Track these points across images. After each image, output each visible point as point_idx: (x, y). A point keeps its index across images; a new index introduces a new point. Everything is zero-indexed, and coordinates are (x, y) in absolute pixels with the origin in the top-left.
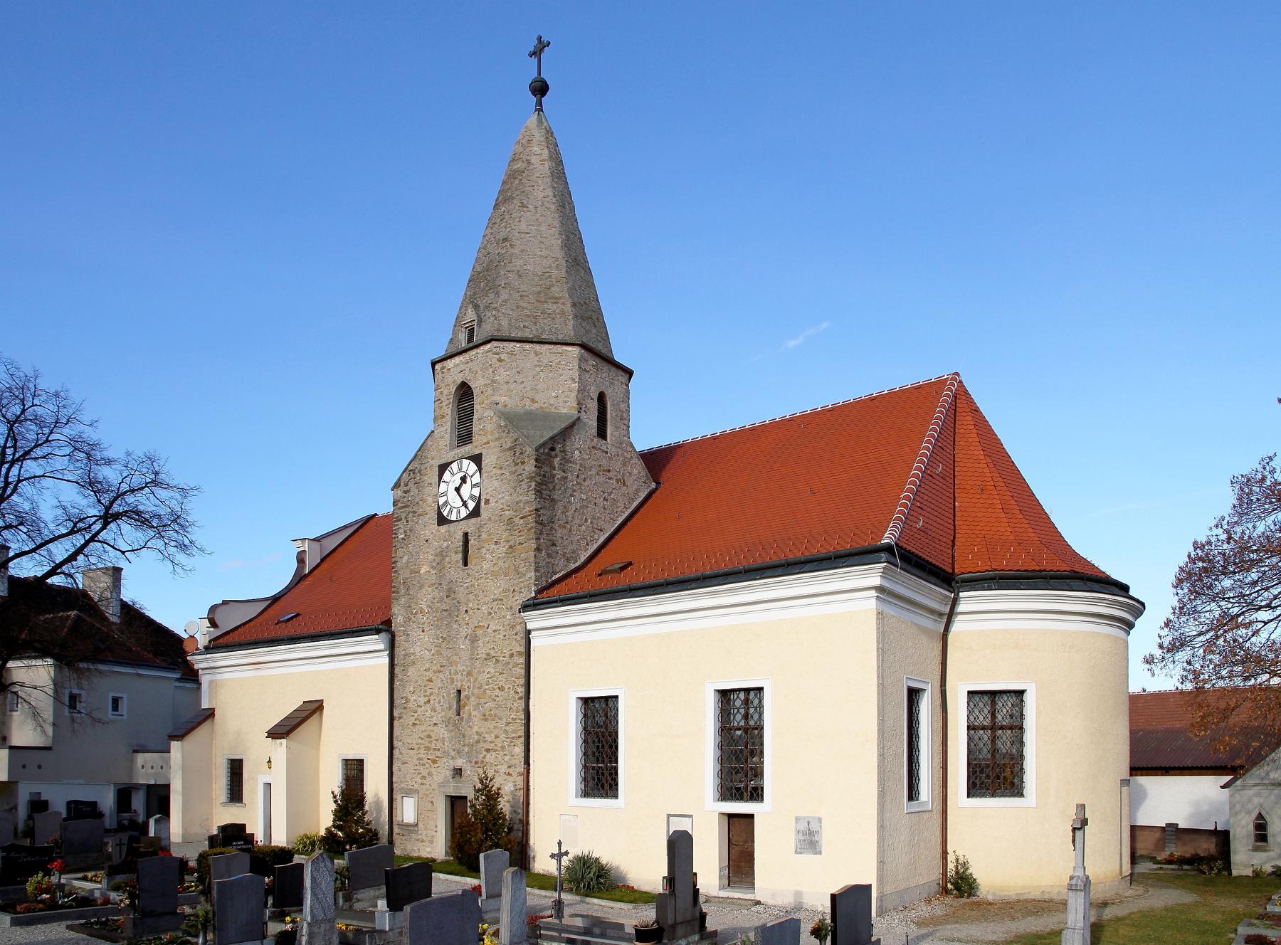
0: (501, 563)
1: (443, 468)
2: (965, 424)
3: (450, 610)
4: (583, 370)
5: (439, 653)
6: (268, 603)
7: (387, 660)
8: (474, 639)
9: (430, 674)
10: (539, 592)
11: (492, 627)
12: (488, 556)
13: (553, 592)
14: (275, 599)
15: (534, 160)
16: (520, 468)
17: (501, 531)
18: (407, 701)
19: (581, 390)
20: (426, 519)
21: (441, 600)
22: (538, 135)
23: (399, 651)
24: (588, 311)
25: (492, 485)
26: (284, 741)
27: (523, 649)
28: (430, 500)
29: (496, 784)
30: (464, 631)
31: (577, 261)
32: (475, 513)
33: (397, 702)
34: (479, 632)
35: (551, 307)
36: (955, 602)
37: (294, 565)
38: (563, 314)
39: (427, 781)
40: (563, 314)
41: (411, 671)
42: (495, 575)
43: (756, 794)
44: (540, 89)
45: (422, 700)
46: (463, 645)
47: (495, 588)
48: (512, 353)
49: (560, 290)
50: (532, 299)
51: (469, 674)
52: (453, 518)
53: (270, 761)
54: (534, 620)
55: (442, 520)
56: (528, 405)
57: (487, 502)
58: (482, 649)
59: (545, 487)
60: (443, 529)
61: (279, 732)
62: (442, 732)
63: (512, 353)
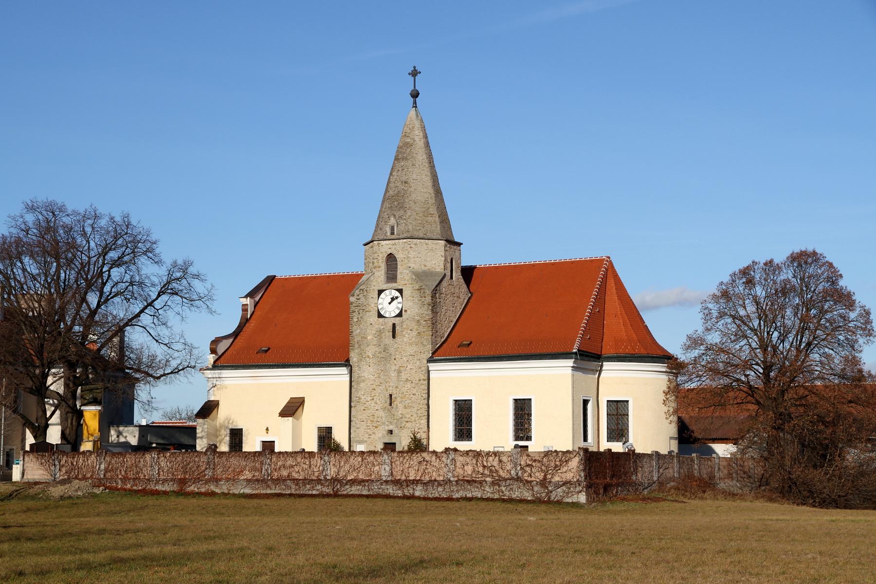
0: (414, 339)
1: (380, 292)
2: (611, 283)
3: (385, 356)
4: (446, 251)
5: (379, 377)
6: (231, 340)
7: (348, 379)
8: (399, 372)
9: (374, 386)
10: (433, 354)
11: (409, 367)
12: (407, 336)
13: (439, 354)
14: (236, 334)
15: (417, 138)
16: (423, 299)
17: (413, 325)
18: (360, 398)
19: (446, 260)
20: (370, 314)
21: (380, 353)
22: (417, 124)
23: (354, 375)
24: (444, 220)
25: (408, 305)
26: (290, 418)
27: (426, 378)
28: (373, 305)
29: (418, 436)
30: (393, 368)
31: (438, 192)
32: (400, 315)
33: (353, 399)
34: (402, 369)
35: (430, 219)
36: (602, 366)
37: (240, 313)
38: (435, 222)
39: (372, 437)
40: (435, 222)
41: (362, 385)
42: (411, 344)
43: (529, 438)
44: (415, 95)
45: (369, 398)
46: (393, 374)
47: (411, 350)
48: (416, 244)
49: (433, 210)
50: (421, 215)
51: (397, 387)
52: (387, 315)
53: (267, 429)
54: (433, 366)
55: (380, 316)
56: (423, 268)
57: (406, 311)
58: (404, 376)
59: (434, 307)
60: (381, 320)
61: (284, 413)
62: (381, 413)
63: (416, 244)
